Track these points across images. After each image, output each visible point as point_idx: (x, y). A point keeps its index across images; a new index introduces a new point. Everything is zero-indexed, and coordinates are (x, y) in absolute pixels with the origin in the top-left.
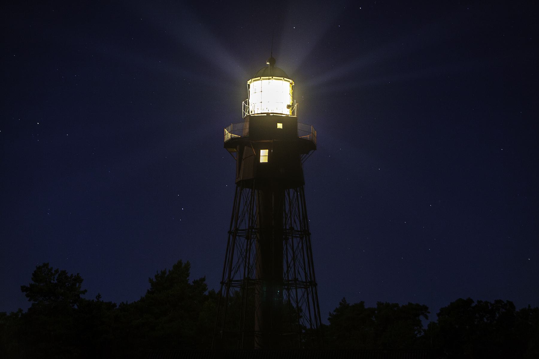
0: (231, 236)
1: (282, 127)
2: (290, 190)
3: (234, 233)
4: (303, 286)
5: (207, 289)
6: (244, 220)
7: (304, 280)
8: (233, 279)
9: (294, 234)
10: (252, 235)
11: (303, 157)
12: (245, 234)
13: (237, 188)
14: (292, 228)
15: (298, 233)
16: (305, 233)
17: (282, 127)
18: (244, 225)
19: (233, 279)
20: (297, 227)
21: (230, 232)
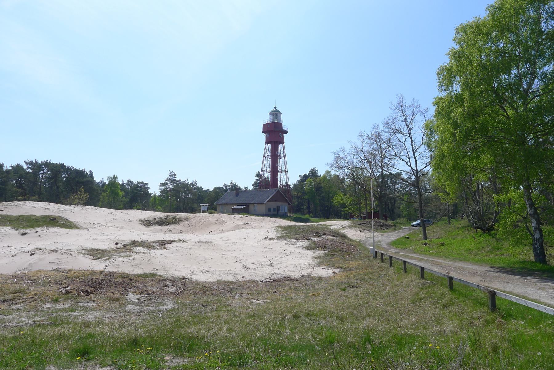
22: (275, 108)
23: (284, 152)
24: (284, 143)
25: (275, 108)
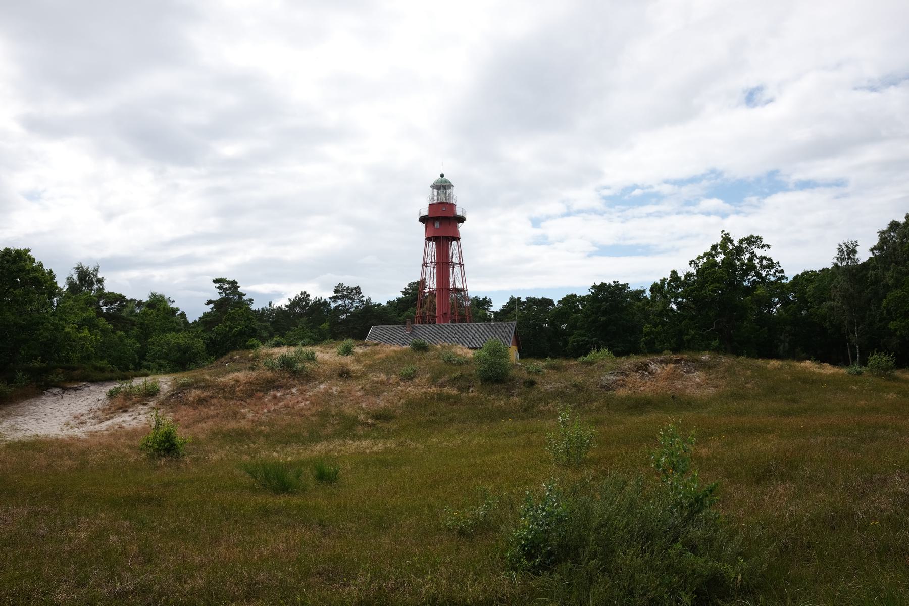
22: (442, 176)
24: (459, 239)
25: (442, 176)
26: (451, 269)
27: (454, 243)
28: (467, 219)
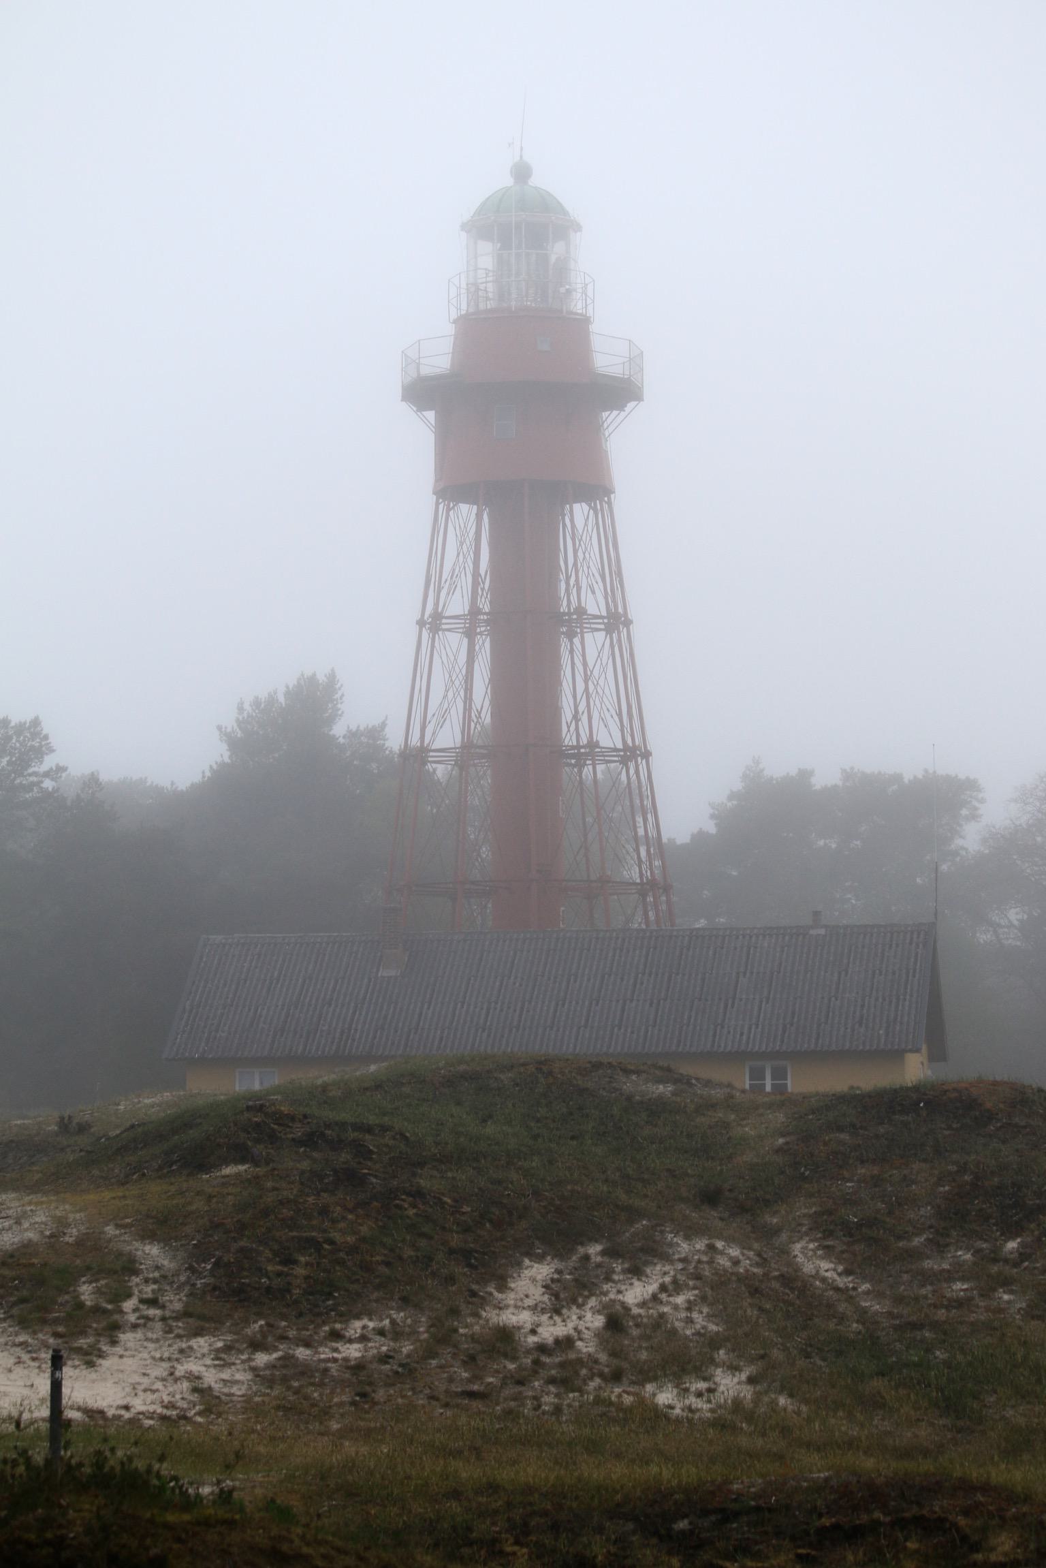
0: (425, 634)
1: (961, 812)
2: (574, 505)
3: (433, 623)
4: (616, 759)
5: (340, 689)
6: (459, 586)
7: (620, 746)
8: (433, 741)
9: (587, 623)
10: (616, 897)
11: (609, 420)
12: (463, 626)
13: (437, 504)
14: (581, 611)
15: (601, 621)
16: (616, 622)
17: (961, 812)
18: (457, 605)
19: (428, 745)
20: (594, 604)
21: (421, 623)
23: (613, 574)
26: (564, 642)
27: (580, 511)
28: (647, 392)
